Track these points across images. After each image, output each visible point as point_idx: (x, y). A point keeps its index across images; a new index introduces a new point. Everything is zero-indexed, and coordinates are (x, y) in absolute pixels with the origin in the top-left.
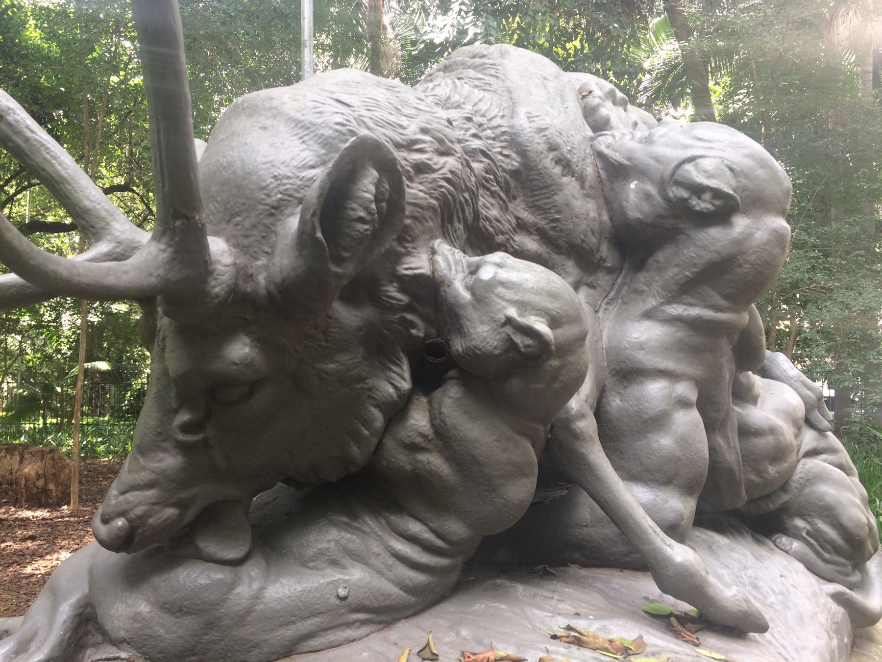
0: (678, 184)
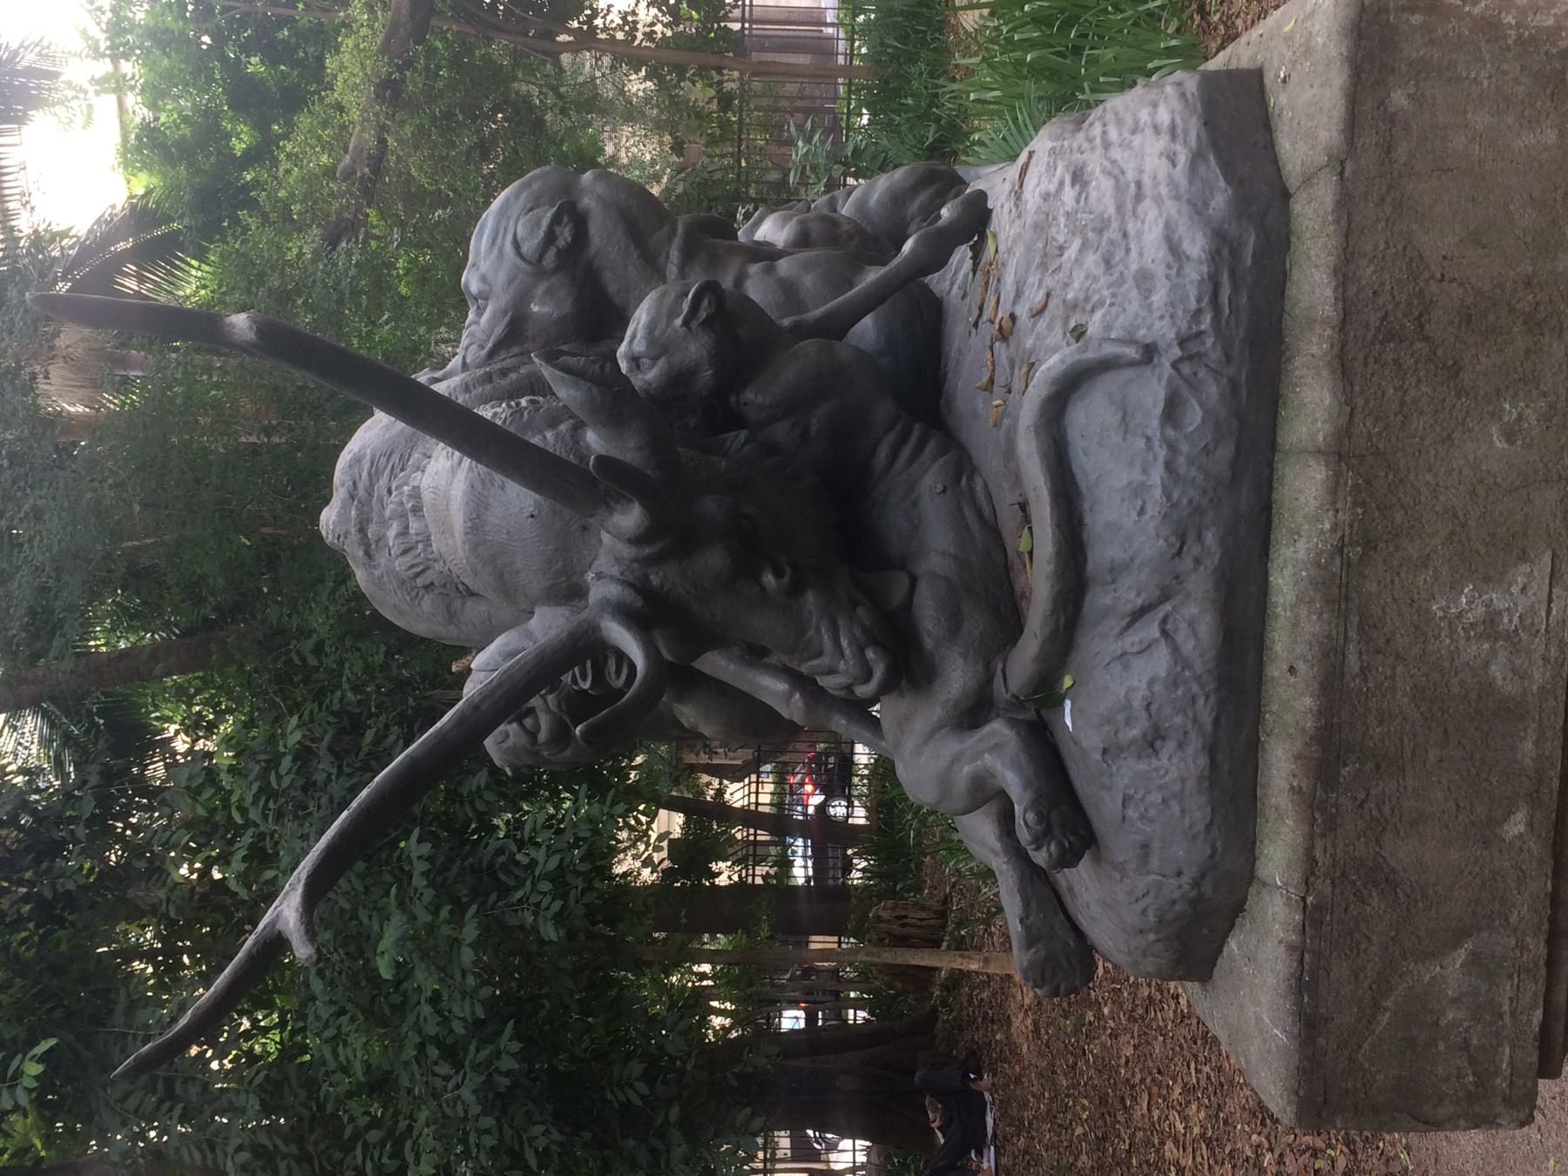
0: (540, 260)
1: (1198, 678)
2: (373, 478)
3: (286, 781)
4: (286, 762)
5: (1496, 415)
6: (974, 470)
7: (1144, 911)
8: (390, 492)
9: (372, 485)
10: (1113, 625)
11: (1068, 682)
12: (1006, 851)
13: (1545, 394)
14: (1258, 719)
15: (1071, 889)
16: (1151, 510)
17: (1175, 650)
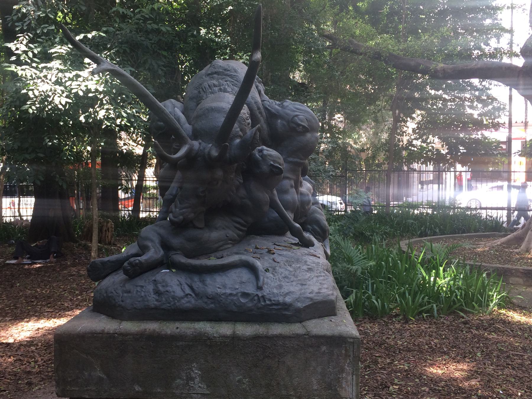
1: (175, 304)
2: (231, 76)
3: (149, 26)
4: (155, 26)
5: (245, 377)
6: (233, 245)
7: (112, 293)
8: (226, 81)
9: (228, 76)
10: (189, 281)
11: (174, 270)
12: (128, 256)
13: (250, 389)
14: (164, 320)
15: (118, 274)
16: (219, 290)
17: (182, 298)
